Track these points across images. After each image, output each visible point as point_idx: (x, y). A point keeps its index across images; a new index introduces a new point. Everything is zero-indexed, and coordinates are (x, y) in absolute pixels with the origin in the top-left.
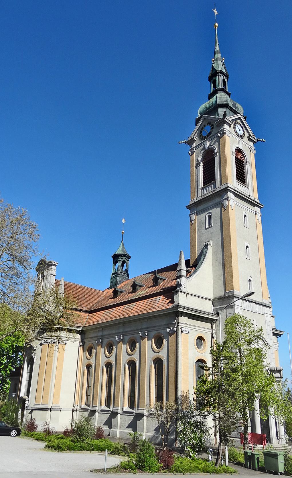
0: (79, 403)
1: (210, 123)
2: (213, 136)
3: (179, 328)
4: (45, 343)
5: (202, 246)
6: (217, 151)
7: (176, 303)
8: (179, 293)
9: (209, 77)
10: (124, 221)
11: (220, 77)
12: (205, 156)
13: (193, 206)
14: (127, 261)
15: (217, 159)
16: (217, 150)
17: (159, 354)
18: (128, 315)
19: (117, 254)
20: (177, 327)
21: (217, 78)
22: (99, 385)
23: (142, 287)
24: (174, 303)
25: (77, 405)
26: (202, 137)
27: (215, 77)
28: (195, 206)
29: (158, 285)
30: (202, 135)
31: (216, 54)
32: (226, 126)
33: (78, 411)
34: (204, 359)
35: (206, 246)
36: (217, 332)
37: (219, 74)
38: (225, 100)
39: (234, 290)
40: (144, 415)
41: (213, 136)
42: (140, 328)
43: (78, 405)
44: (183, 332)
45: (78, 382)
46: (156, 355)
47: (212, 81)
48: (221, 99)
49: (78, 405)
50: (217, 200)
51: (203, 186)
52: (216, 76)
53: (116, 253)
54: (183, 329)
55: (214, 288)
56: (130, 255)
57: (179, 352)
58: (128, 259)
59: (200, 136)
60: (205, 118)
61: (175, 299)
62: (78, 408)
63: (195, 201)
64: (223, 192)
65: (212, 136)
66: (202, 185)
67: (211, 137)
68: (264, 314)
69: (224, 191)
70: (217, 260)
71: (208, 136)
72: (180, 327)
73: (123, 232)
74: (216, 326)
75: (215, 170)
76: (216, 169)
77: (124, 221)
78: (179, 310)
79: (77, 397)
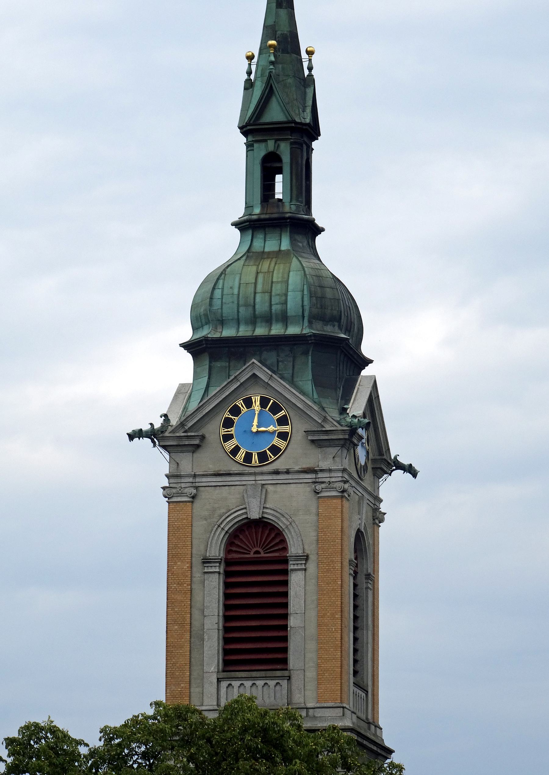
2: (288, 472)
38: (335, 313)
41: (288, 472)
48: (322, 307)
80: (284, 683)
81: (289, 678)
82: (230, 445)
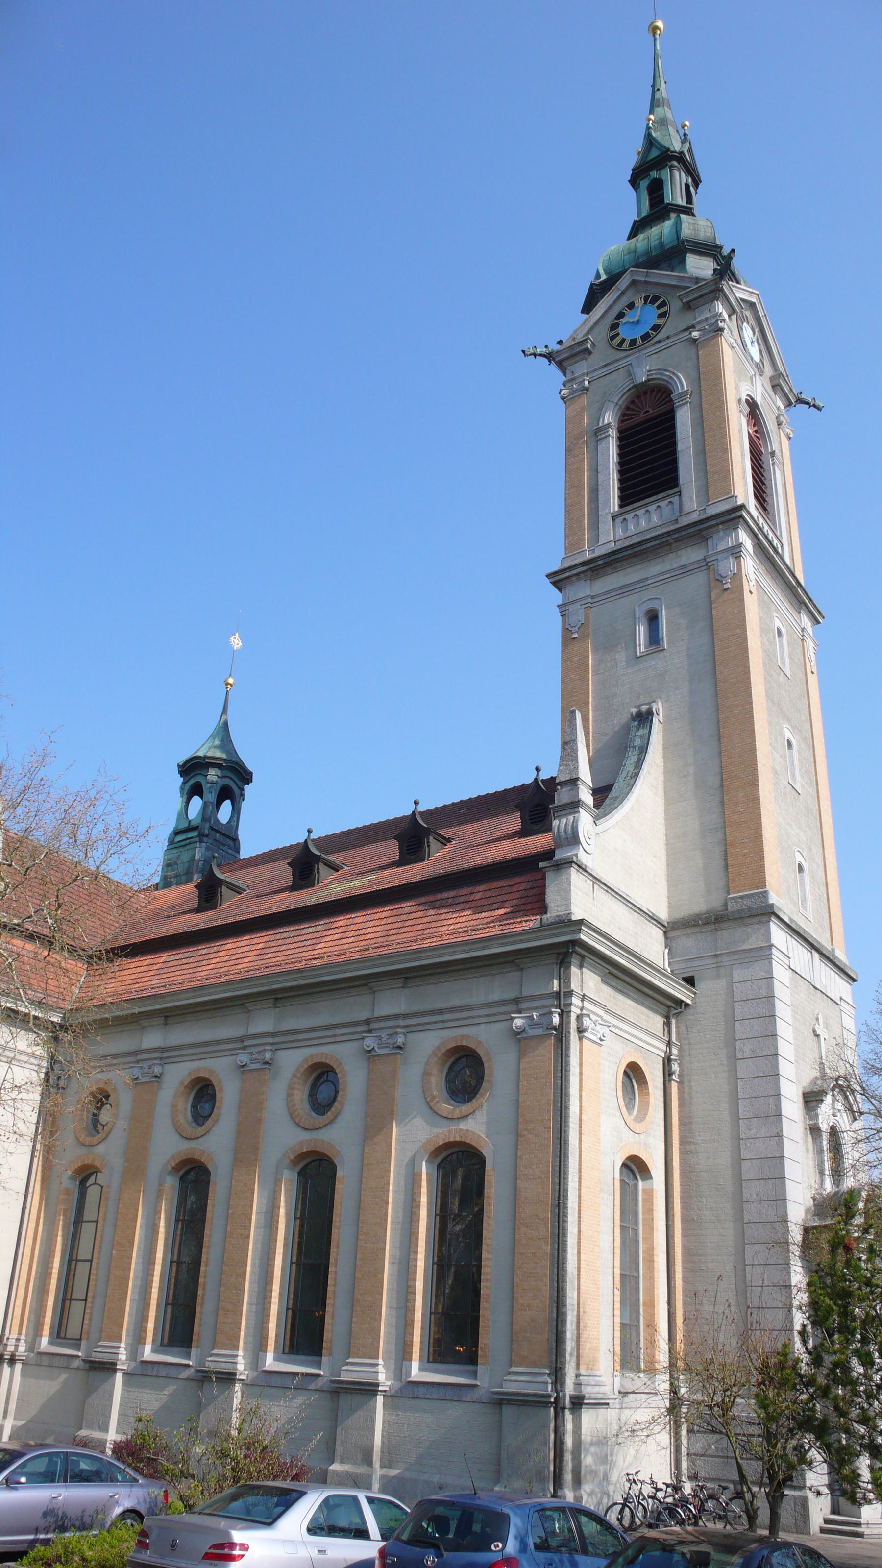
0: (24, 1332)
1: (655, 299)
2: (668, 338)
3: (573, 1017)
4: (257, 1066)
5: (623, 717)
6: (686, 388)
7: (554, 911)
8: (573, 871)
9: (633, 170)
10: (236, 642)
11: (676, 173)
12: (628, 408)
13: (578, 574)
14: (236, 791)
15: (684, 418)
16: (683, 384)
17: (462, 1126)
18: (300, 962)
19: (205, 757)
20: (564, 1014)
21: (665, 174)
22: (134, 1255)
23: (337, 871)
24: (546, 913)
25: (16, 1336)
26: (617, 341)
27: (659, 169)
28: (589, 573)
29: (423, 860)
30: (618, 334)
31: (658, 106)
32: (720, 307)
33: (18, 1366)
34: (644, 1159)
35: (644, 718)
36: (687, 1053)
37: (675, 163)
39: (768, 888)
40: (380, 1388)
41: (668, 338)
42: (365, 1015)
43: (23, 1337)
44: (585, 1034)
45: (29, 1242)
46: (444, 1133)
47: (644, 184)
49: (23, 1337)
50: (691, 555)
51: (621, 506)
52: (664, 167)
53: (201, 754)
54: (586, 1022)
55: (673, 881)
56: (250, 766)
57: (571, 1119)
58: (239, 783)
59: (612, 338)
60: (636, 278)
61: (551, 897)
62: (22, 1348)
63: (587, 556)
64: (718, 525)
65: (664, 340)
66: (614, 504)
67: (659, 342)
68: (839, 1002)
69: (721, 523)
70: (685, 776)
71: (646, 337)
72: (575, 1011)
73: (231, 681)
74: (683, 1029)
75: (674, 452)
76: (680, 446)
77: (236, 642)
78: (582, 937)
79: (19, 1303)
80: (675, 500)
81: (680, 494)
82: (617, 341)
